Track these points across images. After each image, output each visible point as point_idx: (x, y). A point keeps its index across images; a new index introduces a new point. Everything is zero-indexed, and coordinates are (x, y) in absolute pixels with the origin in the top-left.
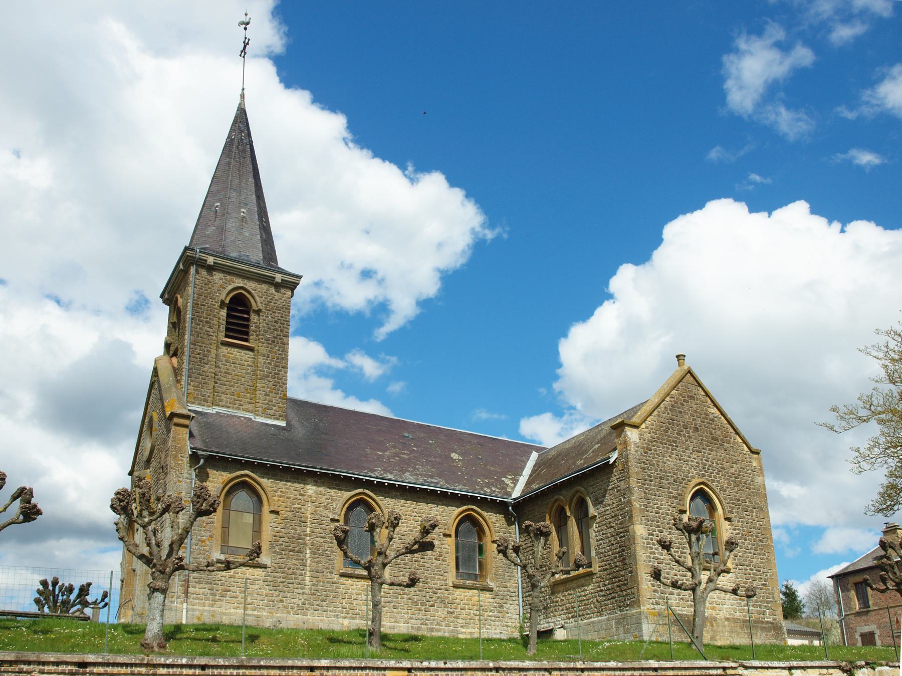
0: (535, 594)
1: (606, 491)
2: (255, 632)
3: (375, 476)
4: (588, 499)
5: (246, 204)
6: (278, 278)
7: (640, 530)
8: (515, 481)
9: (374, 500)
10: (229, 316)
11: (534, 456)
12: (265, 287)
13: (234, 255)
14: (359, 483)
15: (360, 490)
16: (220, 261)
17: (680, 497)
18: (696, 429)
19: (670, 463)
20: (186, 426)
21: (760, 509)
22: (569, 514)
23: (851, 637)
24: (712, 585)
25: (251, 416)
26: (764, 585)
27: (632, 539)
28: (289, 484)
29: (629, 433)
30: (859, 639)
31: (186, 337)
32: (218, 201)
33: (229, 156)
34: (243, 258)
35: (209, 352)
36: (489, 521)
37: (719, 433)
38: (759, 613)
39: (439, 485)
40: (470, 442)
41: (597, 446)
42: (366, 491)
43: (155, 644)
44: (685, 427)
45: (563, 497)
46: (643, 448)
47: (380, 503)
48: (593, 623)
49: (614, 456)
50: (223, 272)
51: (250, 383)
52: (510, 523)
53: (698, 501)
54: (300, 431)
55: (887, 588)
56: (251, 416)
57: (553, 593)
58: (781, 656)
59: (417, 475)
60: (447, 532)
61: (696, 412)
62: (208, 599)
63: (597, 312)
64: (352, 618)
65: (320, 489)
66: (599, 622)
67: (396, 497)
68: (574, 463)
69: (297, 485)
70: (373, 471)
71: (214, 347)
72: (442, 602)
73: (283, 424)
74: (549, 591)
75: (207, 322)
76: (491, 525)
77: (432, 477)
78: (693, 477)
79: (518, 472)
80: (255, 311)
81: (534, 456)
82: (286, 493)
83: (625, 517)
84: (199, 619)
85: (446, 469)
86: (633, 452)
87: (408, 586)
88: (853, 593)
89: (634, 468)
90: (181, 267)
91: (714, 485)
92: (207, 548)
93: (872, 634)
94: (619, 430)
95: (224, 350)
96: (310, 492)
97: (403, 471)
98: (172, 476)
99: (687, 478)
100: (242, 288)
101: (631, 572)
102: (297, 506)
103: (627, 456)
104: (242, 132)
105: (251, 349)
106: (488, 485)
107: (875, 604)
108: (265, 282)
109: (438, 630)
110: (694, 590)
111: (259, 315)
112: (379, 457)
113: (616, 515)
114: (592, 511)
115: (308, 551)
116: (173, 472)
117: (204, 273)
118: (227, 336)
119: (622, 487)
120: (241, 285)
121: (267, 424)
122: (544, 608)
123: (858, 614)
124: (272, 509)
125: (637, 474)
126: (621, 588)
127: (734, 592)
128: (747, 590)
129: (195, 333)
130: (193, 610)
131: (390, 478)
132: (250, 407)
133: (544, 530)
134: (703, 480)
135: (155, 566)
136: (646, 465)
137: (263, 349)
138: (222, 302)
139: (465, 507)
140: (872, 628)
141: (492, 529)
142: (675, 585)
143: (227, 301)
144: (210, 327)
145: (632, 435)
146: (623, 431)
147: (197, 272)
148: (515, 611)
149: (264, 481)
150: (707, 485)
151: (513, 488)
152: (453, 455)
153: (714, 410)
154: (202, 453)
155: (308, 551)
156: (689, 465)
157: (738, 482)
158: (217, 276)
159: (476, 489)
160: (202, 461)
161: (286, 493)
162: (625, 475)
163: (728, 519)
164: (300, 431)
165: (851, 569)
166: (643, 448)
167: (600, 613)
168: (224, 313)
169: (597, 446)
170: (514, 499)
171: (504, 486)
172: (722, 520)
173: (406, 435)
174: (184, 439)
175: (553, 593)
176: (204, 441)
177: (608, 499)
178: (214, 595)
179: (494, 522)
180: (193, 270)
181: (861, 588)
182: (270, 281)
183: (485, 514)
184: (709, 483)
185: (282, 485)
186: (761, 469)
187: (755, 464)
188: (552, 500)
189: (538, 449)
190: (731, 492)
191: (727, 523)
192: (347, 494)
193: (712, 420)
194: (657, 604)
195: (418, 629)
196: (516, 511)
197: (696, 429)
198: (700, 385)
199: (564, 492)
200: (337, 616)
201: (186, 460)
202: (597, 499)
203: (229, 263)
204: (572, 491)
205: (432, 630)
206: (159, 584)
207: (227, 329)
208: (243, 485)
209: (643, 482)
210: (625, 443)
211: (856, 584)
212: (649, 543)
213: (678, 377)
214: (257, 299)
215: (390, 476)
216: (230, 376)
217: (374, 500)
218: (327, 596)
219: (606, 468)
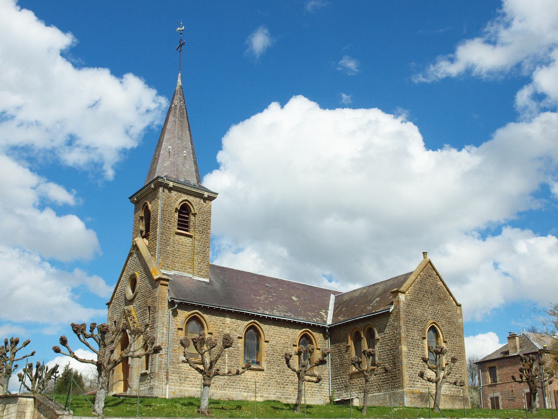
0: (367, 384)
1: (386, 326)
2: (238, 404)
3: (260, 312)
4: (375, 329)
5: (186, 148)
6: (206, 194)
7: (404, 348)
8: (327, 314)
9: (259, 326)
10: (179, 216)
11: (332, 297)
12: (198, 199)
13: (182, 180)
14: (253, 317)
15: (253, 321)
16: (176, 185)
17: (423, 330)
18: (432, 294)
19: (419, 312)
20: (167, 285)
21: (460, 336)
22: (363, 336)
23: (485, 399)
24: (445, 380)
25: (191, 276)
26: (460, 377)
27: (400, 353)
28: (217, 317)
29: (400, 296)
30: (490, 401)
31: (158, 230)
32: (170, 145)
33: (174, 116)
34: (187, 182)
35: (170, 238)
36: (316, 337)
37: (442, 295)
38: (458, 391)
39: (291, 317)
40: (299, 289)
41: (378, 299)
42: (256, 321)
43: (206, 412)
44: (426, 292)
45: (359, 326)
46: (407, 304)
47: (262, 327)
48: (375, 396)
49: (392, 308)
50: (177, 191)
51: (190, 257)
52: (326, 338)
53: (431, 332)
54: (217, 285)
55: (522, 381)
56: (191, 276)
57: (351, 379)
58: (474, 415)
59: (279, 311)
60: (295, 344)
61: (432, 284)
62: (177, 382)
63: (253, 118)
64: (248, 392)
65: (233, 320)
66: (379, 395)
67: (270, 324)
68: (365, 308)
69: (221, 318)
70: (259, 309)
71: (172, 235)
72: (291, 383)
73: (207, 280)
74: (348, 377)
75: (168, 221)
76: (316, 339)
77: (287, 312)
78: (429, 320)
79: (327, 308)
80: (193, 214)
81: (332, 297)
82: (216, 322)
83: (396, 341)
84: (174, 394)
85: (292, 308)
86: (402, 306)
87: (316, 382)
88: (488, 373)
89: (402, 315)
90: (153, 186)
91: (439, 324)
92: (177, 354)
93: (497, 398)
94: (395, 294)
95: (177, 237)
96: (228, 322)
97: (273, 309)
98: (160, 314)
99: (427, 320)
100: (187, 200)
101: (399, 370)
102: (221, 330)
103: (399, 309)
104: (181, 101)
105: (190, 237)
106: (315, 317)
107: (500, 380)
108: (198, 197)
109: (290, 398)
110: (436, 383)
111: (195, 216)
112: (259, 300)
113: (391, 340)
114: (377, 336)
115: (227, 355)
116: (160, 311)
117: (166, 191)
118: (178, 229)
119: (395, 325)
120: (186, 199)
121: (200, 281)
122: (345, 387)
123: (490, 386)
124: (209, 332)
125: (404, 318)
126: (392, 376)
127: (455, 383)
128: (460, 382)
129: (163, 228)
130: (172, 389)
131: (267, 313)
132: (190, 270)
133: (373, 353)
134: (434, 321)
135: (205, 373)
136: (408, 313)
137: (197, 237)
138: (176, 209)
139: (304, 330)
140: (497, 394)
141: (317, 342)
142: (429, 380)
143: (179, 209)
144: (170, 224)
145: (402, 297)
146: (397, 295)
147: (163, 191)
148: (326, 386)
149: (205, 316)
150: (436, 324)
151: (327, 318)
152: (293, 298)
153: (440, 283)
154: (176, 301)
155: (227, 355)
156: (427, 313)
157: (450, 322)
158: (174, 193)
159: (309, 319)
160: (176, 305)
161: (216, 322)
162: (397, 318)
163: (445, 342)
164: (217, 285)
165: (488, 359)
166: (407, 304)
167: (380, 391)
168: (176, 215)
169: (378, 299)
170: (329, 325)
171: (322, 318)
172: (442, 342)
173: (268, 285)
174: (165, 293)
175: (351, 379)
176: (175, 294)
177: (387, 330)
178: (180, 380)
179: (318, 337)
180: (161, 189)
181: (492, 371)
182: (201, 196)
183: (313, 333)
184: (437, 323)
185: (215, 318)
186: (461, 315)
187: (458, 312)
188: (353, 328)
189: (334, 293)
190: (447, 327)
191: (445, 344)
192: (246, 323)
193: (439, 288)
194: (411, 387)
195: (280, 398)
196: (332, 333)
197: (432, 294)
198: (434, 269)
199: (360, 324)
200: (240, 391)
201: (167, 304)
202: (380, 330)
203: (181, 186)
204: (366, 324)
205: (287, 398)
206: (207, 382)
207: (179, 225)
208: (194, 318)
209: (406, 322)
210: (398, 301)
211: (490, 368)
212: (408, 355)
213: (424, 265)
214: (195, 207)
215: (267, 313)
216: (180, 253)
217: (259, 326)
218: (236, 380)
219: (387, 314)
